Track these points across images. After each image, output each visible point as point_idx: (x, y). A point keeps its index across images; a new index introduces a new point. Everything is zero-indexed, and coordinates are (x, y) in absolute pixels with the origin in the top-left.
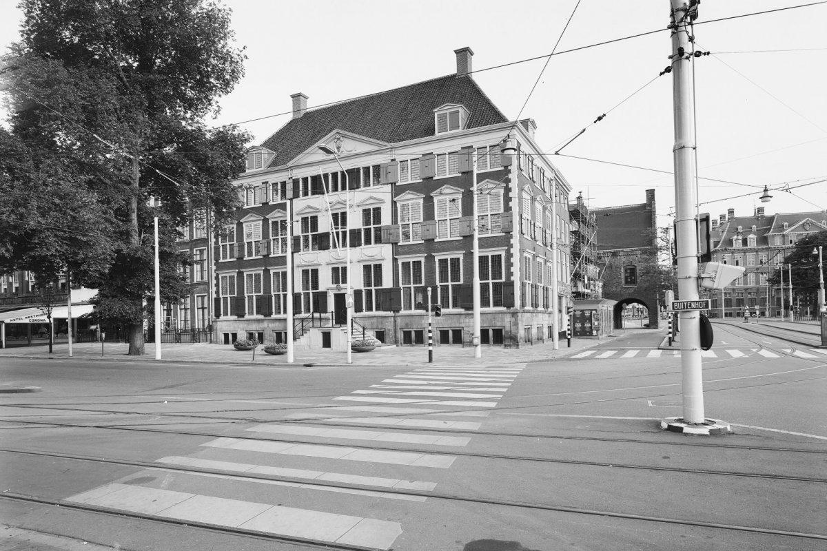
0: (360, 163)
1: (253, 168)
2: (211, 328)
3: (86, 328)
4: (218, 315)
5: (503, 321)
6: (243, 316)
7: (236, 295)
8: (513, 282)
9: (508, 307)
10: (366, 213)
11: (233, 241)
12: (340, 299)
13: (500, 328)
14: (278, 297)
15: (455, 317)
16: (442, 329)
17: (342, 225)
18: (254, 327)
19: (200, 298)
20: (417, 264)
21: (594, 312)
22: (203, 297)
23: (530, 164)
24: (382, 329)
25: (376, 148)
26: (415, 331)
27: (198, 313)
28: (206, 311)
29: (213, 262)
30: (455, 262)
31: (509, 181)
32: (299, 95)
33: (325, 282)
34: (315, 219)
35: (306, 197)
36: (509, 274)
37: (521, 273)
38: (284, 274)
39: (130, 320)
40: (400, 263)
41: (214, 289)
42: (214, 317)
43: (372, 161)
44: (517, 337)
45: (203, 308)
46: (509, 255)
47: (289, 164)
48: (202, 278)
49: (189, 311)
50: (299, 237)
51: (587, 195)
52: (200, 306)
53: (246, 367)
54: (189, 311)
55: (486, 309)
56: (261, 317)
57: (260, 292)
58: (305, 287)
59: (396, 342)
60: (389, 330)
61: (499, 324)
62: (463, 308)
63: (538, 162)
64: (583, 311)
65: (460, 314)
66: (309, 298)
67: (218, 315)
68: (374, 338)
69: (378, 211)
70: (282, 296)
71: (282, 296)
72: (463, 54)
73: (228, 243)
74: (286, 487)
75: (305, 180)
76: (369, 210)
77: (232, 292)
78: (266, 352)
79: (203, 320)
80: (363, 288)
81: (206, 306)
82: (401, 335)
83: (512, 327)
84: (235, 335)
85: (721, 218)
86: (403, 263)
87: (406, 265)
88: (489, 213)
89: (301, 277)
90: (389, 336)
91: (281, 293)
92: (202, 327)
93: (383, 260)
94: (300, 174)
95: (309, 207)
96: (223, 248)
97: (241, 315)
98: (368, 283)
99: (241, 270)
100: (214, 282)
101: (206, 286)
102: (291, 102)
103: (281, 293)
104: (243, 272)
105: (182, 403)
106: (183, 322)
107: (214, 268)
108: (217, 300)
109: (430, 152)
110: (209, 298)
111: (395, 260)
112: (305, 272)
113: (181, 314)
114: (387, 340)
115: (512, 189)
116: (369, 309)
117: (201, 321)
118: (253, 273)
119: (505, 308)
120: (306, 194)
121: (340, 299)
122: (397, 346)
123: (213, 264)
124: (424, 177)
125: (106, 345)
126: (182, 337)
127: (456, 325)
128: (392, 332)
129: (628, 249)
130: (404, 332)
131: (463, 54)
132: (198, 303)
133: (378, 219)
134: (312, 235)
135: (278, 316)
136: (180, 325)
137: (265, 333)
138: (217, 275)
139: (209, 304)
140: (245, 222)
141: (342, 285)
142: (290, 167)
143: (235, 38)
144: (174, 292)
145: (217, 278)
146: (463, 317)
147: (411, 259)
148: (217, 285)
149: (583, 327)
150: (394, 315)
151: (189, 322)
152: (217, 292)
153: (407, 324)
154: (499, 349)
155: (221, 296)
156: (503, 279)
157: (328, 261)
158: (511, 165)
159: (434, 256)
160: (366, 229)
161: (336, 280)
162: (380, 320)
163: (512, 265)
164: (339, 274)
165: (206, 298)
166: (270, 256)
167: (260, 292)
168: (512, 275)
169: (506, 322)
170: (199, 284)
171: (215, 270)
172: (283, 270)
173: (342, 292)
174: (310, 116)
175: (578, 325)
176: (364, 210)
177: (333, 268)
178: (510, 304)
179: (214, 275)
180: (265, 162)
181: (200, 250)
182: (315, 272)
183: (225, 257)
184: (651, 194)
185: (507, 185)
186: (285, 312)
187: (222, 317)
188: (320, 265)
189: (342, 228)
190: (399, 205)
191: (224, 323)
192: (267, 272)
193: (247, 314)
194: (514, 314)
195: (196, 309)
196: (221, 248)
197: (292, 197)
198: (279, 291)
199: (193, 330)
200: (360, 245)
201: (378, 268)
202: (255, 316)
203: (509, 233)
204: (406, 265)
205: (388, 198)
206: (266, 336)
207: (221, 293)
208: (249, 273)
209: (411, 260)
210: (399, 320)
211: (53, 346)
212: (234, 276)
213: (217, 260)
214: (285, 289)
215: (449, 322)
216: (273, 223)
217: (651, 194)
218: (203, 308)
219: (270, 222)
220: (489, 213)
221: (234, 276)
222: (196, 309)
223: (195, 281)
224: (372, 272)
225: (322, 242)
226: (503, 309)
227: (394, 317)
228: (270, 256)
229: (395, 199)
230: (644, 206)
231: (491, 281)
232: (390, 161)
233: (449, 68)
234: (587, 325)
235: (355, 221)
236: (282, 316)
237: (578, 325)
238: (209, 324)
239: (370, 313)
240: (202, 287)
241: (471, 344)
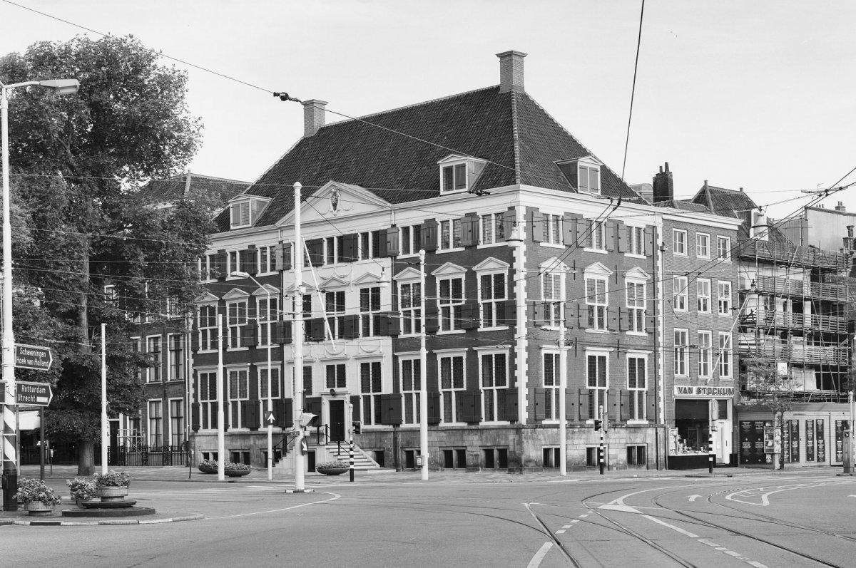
0: (357, 228)
1: (238, 224)
2: (187, 445)
3: (32, 444)
4: (196, 428)
5: (507, 438)
6: (477, 422)
7: (248, 399)
12: (337, 407)
13: (504, 448)
14: (409, 397)
15: (458, 434)
16: (445, 449)
17: (453, 297)
19: (175, 404)
20: (458, 361)
21: (767, 424)
22: (179, 401)
24: (380, 448)
28: (182, 421)
29: (191, 353)
35: (367, 261)
36: (513, 379)
38: (213, 376)
39: (79, 435)
41: (192, 391)
42: (191, 431)
43: (370, 226)
44: (521, 460)
45: (179, 418)
46: (513, 355)
47: (279, 224)
48: (157, 377)
49: (161, 421)
51: (387, 306)
52: (175, 415)
54: (161, 421)
57: (246, 397)
58: (365, 388)
60: (388, 449)
61: (503, 443)
62: (247, 427)
64: (753, 423)
65: (463, 430)
66: (492, 399)
67: (196, 428)
68: (372, 459)
70: (414, 397)
71: (414, 397)
73: (451, 305)
75: (331, 240)
77: (458, 383)
78: (201, 469)
79: (179, 434)
80: (361, 394)
81: (161, 415)
83: (516, 447)
84: (462, 453)
86: (404, 362)
87: (204, 376)
89: (360, 374)
91: (413, 391)
92: (177, 445)
93: (381, 357)
95: (368, 275)
96: (262, 328)
97: (474, 420)
99: (254, 364)
100: (192, 381)
101: (181, 387)
103: (413, 391)
104: (256, 367)
106: (154, 437)
107: (192, 361)
110: (185, 403)
111: (395, 358)
112: (365, 367)
114: (386, 463)
117: (176, 436)
118: (238, 370)
120: (331, 260)
121: (337, 407)
122: (397, 470)
123: (190, 356)
125: (54, 467)
126: (150, 458)
128: (391, 453)
130: (407, 452)
132: (172, 410)
134: (496, 303)
135: (449, 425)
136: (150, 442)
137: (252, 452)
138: (196, 371)
139: (185, 414)
140: (480, 271)
141: (337, 390)
142: (280, 228)
143: (159, 52)
145: (195, 376)
146: (466, 433)
147: (451, 354)
148: (195, 386)
150: (393, 430)
151: (162, 437)
152: (195, 396)
153: (408, 442)
155: (200, 401)
156: (507, 386)
157: (322, 356)
159: (435, 354)
160: (363, 316)
162: (378, 436)
164: (337, 374)
165: (182, 403)
166: (257, 348)
167: (246, 397)
170: (173, 384)
172: (417, 358)
173: (338, 398)
175: (747, 445)
176: (362, 290)
177: (328, 366)
179: (192, 372)
180: (254, 216)
181: (154, 338)
182: (342, 369)
183: (205, 347)
185: (512, 266)
186: (419, 421)
187: (201, 431)
188: (312, 362)
189: (454, 302)
191: (204, 439)
192: (472, 355)
193: (443, 421)
194: (518, 430)
195: (170, 419)
197: (281, 268)
199: (166, 447)
201: (377, 366)
203: (513, 327)
204: (446, 361)
205: (387, 276)
207: (199, 396)
208: (407, 358)
209: (452, 356)
210: (400, 436)
212: (245, 372)
213: (195, 349)
214: (214, 396)
215: (452, 439)
216: (403, 286)
218: (179, 418)
219: (257, 301)
221: (245, 372)
222: (170, 419)
223: (148, 381)
225: (348, 329)
226: (507, 423)
227: (395, 433)
228: (257, 348)
232: (390, 227)
238: (185, 439)
239: (490, 424)
240: (177, 387)
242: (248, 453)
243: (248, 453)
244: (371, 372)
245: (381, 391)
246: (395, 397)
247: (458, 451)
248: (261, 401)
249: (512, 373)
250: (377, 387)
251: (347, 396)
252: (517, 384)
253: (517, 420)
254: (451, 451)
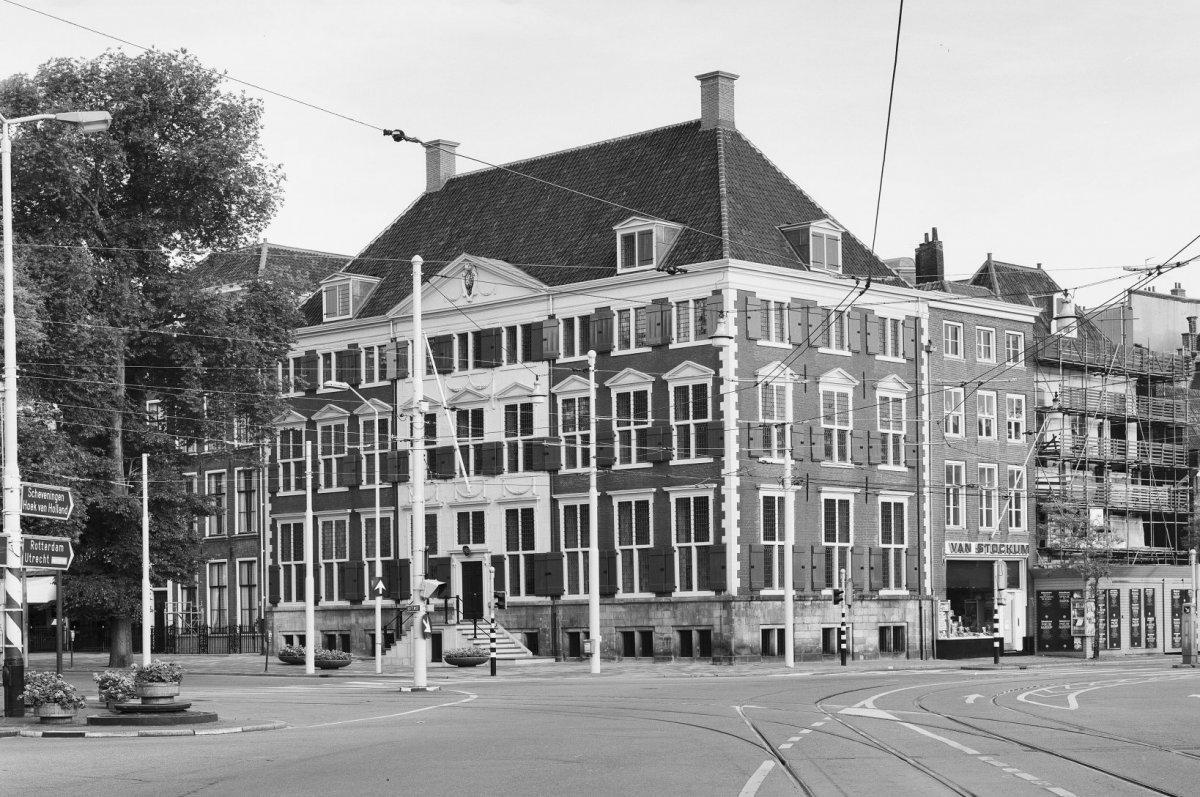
0: (500, 319)
1: (334, 314)
2: (263, 625)
3: (45, 624)
4: (274, 601)
5: (710, 615)
6: (669, 593)
7: (347, 560)
12: (472, 572)
13: (707, 628)
14: (573, 557)
15: (642, 608)
16: (624, 630)
17: (636, 416)
19: (245, 567)
20: (642, 506)
21: (1075, 596)
22: (250, 563)
24: (533, 629)
28: (256, 591)
29: (268, 495)
35: (514, 366)
36: (720, 532)
38: (299, 528)
39: (110, 611)
41: (269, 548)
42: (268, 604)
43: (518, 317)
44: (730, 645)
45: (250, 586)
46: (720, 498)
47: (390, 314)
48: (220, 529)
49: (226, 591)
51: (543, 430)
52: (245, 582)
54: (226, 591)
57: (345, 557)
58: (511, 544)
60: (545, 631)
61: (705, 621)
62: (347, 600)
64: (1055, 593)
65: (649, 603)
66: (689, 560)
67: (274, 601)
68: (521, 645)
70: (581, 557)
71: (581, 557)
73: (632, 428)
75: (463, 337)
77: (643, 538)
79: (251, 609)
80: (506, 554)
81: (225, 582)
83: (724, 627)
84: (647, 636)
86: (566, 507)
87: (286, 527)
89: (504, 524)
91: (579, 549)
92: (248, 624)
93: (535, 501)
95: (517, 386)
96: (368, 461)
97: (664, 590)
99: (357, 510)
100: (269, 535)
101: (253, 543)
103: (579, 549)
104: (358, 514)
106: (216, 613)
107: (269, 507)
110: (259, 566)
111: (554, 503)
112: (511, 515)
114: (541, 650)
117: (247, 612)
118: (334, 519)
120: (464, 365)
121: (472, 572)
122: (557, 660)
123: (267, 500)
125: (76, 656)
126: (211, 643)
128: (549, 635)
130: (570, 634)
132: (241, 575)
134: (695, 424)
135: (629, 596)
136: (211, 620)
137: (353, 634)
138: (274, 521)
139: (259, 582)
140: (673, 380)
141: (472, 547)
142: (393, 320)
143: (222, 73)
145: (273, 527)
146: (654, 607)
147: (633, 497)
148: (273, 541)
150: (550, 603)
151: (227, 614)
152: (274, 555)
153: (571, 621)
155: (280, 563)
156: (711, 542)
157: (451, 500)
159: (610, 497)
160: (509, 443)
162: (531, 611)
164: (472, 525)
165: (256, 566)
166: (361, 488)
167: (345, 557)
168: (724, 501)
170: (242, 539)
172: (584, 502)
173: (474, 559)
175: (1047, 625)
176: (508, 408)
177: (459, 514)
179: (268, 521)
180: (356, 303)
181: (216, 474)
182: (479, 517)
183: (287, 487)
185: (717, 373)
186: (587, 590)
187: (282, 604)
188: (438, 508)
189: (636, 424)
191: (286, 616)
192: (662, 498)
193: (621, 591)
194: (727, 603)
195: (238, 588)
197: (394, 376)
199: (232, 627)
201: (528, 514)
203: (719, 459)
204: (625, 507)
205: (543, 387)
207: (279, 556)
208: (570, 503)
209: (633, 500)
210: (560, 612)
212: (344, 522)
213: (273, 490)
214: (299, 555)
215: (634, 616)
216: (565, 401)
218: (250, 586)
219: (361, 423)
221: (344, 522)
222: (238, 588)
223: (207, 534)
225: (488, 462)
226: (710, 594)
227: (554, 607)
228: (361, 488)
232: (546, 318)
238: (260, 617)
239: (687, 594)
240: (248, 543)
242: (348, 636)
243: (348, 636)
244: (520, 522)
245: (533, 549)
246: (554, 557)
247: (642, 633)
248: (366, 563)
249: (718, 523)
250: (529, 543)
251: (486, 555)
252: (724, 539)
253: (725, 590)
254: (632, 633)
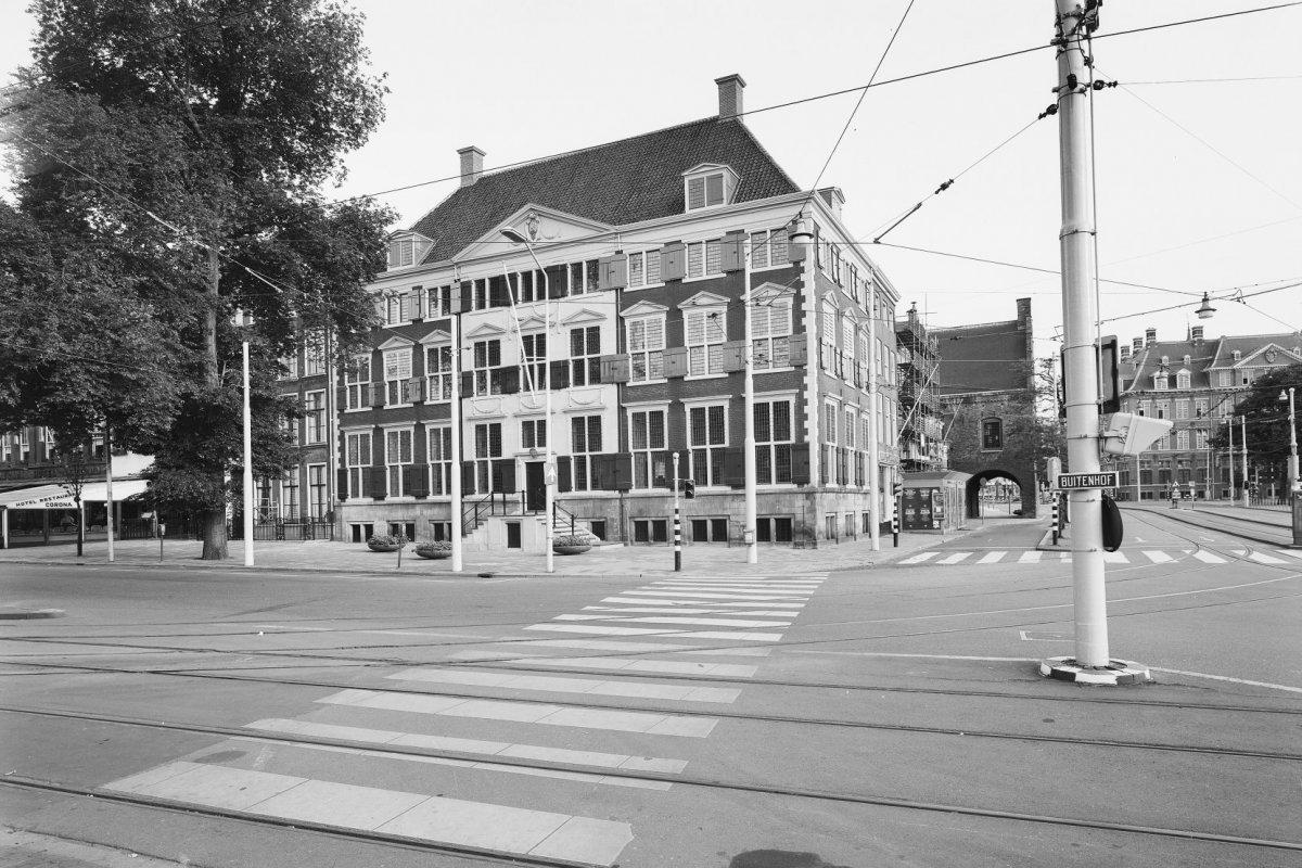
0: (567, 257)
1: (398, 264)
2: (331, 517)
3: (136, 516)
4: (343, 497)
5: (792, 505)
6: (382, 498)
7: (371, 465)
8: (808, 444)
9: (801, 483)
10: (577, 335)
11: (367, 380)
12: (536, 470)
13: (787, 517)
14: (438, 467)
15: (717, 500)
16: (696, 518)
17: (538, 355)
18: (400, 515)
19: (315, 470)
20: (657, 416)
21: (934, 491)
22: (320, 467)
23: (835, 258)
24: (601, 518)
25: (592, 233)
26: (653, 521)
27: (312, 493)
28: (325, 490)
29: (336, 412)
30: (717, 413)
31: (802, 284)
32: (470, 150)
33: (512, 444)
34: (495, 345)
35: (482, 311)
36: (802, 432)
37: (819, 431)
38: (448, 432)
39: (204, 504)
40: (629, 414)
41: (338, 455)
42: (337, 499)
43: (586, 254)
44: (814, 532)
45: (320, 486)
46: (801, 402)
47: (456, 259)
48: (318, 437)
49: (297, 491)
50: (470, 373)
51: (924, 307)
52: (315, 483)
53: (387, 579)
54: (297, 491)
55: (765, 487)
56: (411, 499)
57: (410, 460)
58: (481, 451)
59: (623, 539)
60: (613, 520)
61: (785, 510)
62: (729, 485)
63: (847, 255)
64: (917, 490)
65: (725, 495)
66: (486, 470)
67: (343, 497)
68: (588, 532)
69: (594, 333)
70: (443, 467)
71: (443, 467)
72: (730, 86)
73: (358, 383)
74: (451, 767)
75: (480, 283)
76: (582, 330)
77: (365, 460)
79: (320, 504)
80: (571, 454)
81: (324, 481)
82: (631, 528)
83: (806, 516)
84: (369, 528)
85: (1135, 343)
86: (634, 415)
87: (639, 418)
88: (770, 336)
89: (474, 437)
90: (613, 530)
91: (443, 462)
92: (317, 516)
93: (603, 409)
94: (472, 274)
95: (486, 326)
96: (351, 391)
97: (379, 496)
98: (579, 446)
99: (380, 426)
100: (337, 444)
101: (324, 451)
102: (459, 161)
103: (443, 462)
104: (382, 429)
105: (287, 635)
106: (288, 508)
107: (337, 422)
108: (342, 473)
109: (677, 239)
110: (329, 469)
111: (622, 410)
112: (481, 429)
113: (285, 495)
114: (609, 536)
115: (807, 298)
116: (582, 486)
117: (317, 506)
118: (399, 430)
119: (796, 486)
120: (481, 306)
121: (536, 470)
122: (626, 545)
123: (335, 416)
124: (668, 279)
125: (167, 543)
126: (287, 531)
127: (718, 512)
128: (617, 524)
129: (988, 393)
130: (636, 523)
131: (730, 86)
132: (311, 477)
133: (595, 345)
134: (492, 370)
135: (438, 498)
136: (284, 513)
137: (417, 524)
138: (342, 433)
139: (328, 479)
140: (385, 350)
141: (538, 450)
142: (456, 264)
143: (369, 60)
144: (274, 461)
145: (342, 438)
146: (729, 499)
147: (647, 408)
148: (342, 449)
149: (918, 516)
150: (620, 496)
151: (298, 508)
152: (342, 460)
153: (640, 511)
154: (785, 550)
155: (348, 466)
156: (793, 440)
157: (516, 411)
158: (804, 260)
159: (683, 404)
160: (576, 361)
161: (528, 441)
162: (598, 504)
163: (806, 417)
164: (534, 432)
165: (324, 470)
166: (425, 403)
167: (410, 460)
168: (807, 434)
169: (796, 508)
170: (313, 447)
171: (339, 426)
172: (446, 426)
173: (539, 459)
174: (488, 183)
175: (910, 512)
176: (573, 331)
177: (524, 423)
178: (803, 480)
179: (337, 433)
180: (417, 255)
181: (315, 394)
182: (496, 429)
183: (354, 405)
184: (1025, 305)
185: (799, 292)
186: (449, 491)
187: (350, 500)
188: (503, 417)
189: (538, 360)
190: (627, 323)
191: (353, 509)
192: (420, 428)
193: (389, 495)
194: (810, 495)
195: (309, 487)
196: (348, 391)
197: (459, 310)
198: (439, 458)
199: (304, 519)
200: (566, 385)
201: (596, 422)
202: (401, 498)
203: (801, 366)
204: (639, 418)
205: (610, 312)
206: (419, 529)
207: (347, 461)
208: (392, 430)
209: (647, 410)
210: (628, 504)
211: (84, 546)
212: (368, 435)
213: (341, 409)
214: (448, 455)
215: (707, 507)
216: (430, 351)
217: (1025, 305)
218: (320, 486)
219: (425, 350)
220: (770, 336)
221: (368, 435)
222: (309, 487)
223: (307, 443)
224: (586, 429)
225: (507, 381)
226: (792, 487)
227: (621, 499)
228: (425, 403)
229: (622, 314)
230: (1014, 325)
231: (772, 443)
232: (614, 253)
233: (707, 106)
234: (925, 512)
235: (559, 348)
236: (444, 497)
237: (910, 512)
238: (329, 511)
239: (582, 494)
240: (318, 452)
241: (741, 541)
